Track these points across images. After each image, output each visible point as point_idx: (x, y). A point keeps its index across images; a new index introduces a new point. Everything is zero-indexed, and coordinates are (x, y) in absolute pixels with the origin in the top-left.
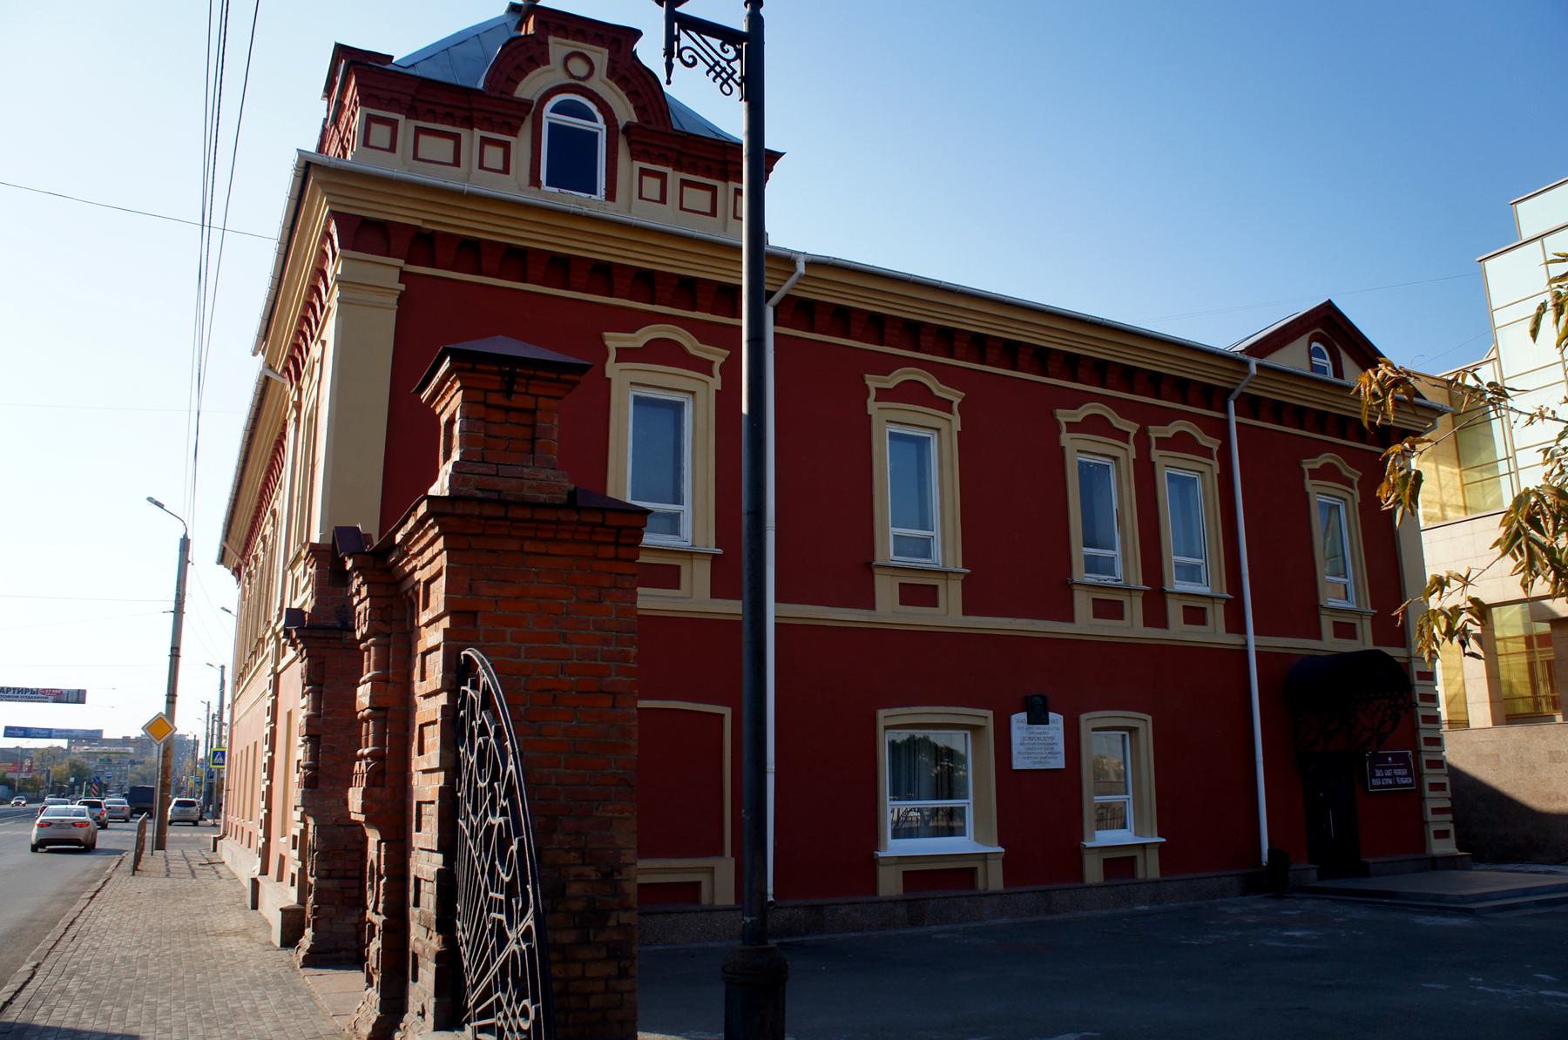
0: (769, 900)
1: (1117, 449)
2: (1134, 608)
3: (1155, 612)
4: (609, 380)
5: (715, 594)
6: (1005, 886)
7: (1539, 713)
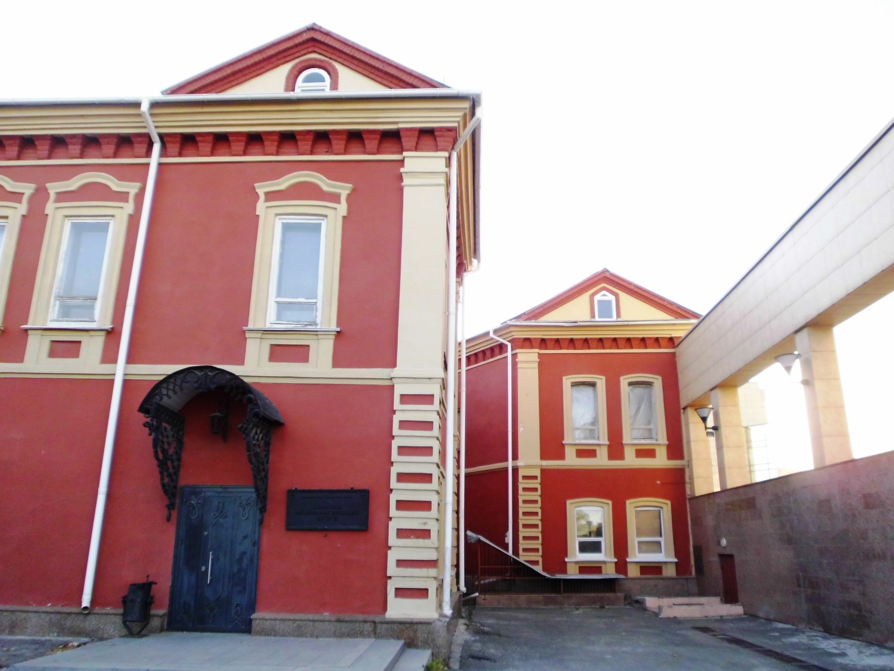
0: (48, 185)
5: (337, 363)
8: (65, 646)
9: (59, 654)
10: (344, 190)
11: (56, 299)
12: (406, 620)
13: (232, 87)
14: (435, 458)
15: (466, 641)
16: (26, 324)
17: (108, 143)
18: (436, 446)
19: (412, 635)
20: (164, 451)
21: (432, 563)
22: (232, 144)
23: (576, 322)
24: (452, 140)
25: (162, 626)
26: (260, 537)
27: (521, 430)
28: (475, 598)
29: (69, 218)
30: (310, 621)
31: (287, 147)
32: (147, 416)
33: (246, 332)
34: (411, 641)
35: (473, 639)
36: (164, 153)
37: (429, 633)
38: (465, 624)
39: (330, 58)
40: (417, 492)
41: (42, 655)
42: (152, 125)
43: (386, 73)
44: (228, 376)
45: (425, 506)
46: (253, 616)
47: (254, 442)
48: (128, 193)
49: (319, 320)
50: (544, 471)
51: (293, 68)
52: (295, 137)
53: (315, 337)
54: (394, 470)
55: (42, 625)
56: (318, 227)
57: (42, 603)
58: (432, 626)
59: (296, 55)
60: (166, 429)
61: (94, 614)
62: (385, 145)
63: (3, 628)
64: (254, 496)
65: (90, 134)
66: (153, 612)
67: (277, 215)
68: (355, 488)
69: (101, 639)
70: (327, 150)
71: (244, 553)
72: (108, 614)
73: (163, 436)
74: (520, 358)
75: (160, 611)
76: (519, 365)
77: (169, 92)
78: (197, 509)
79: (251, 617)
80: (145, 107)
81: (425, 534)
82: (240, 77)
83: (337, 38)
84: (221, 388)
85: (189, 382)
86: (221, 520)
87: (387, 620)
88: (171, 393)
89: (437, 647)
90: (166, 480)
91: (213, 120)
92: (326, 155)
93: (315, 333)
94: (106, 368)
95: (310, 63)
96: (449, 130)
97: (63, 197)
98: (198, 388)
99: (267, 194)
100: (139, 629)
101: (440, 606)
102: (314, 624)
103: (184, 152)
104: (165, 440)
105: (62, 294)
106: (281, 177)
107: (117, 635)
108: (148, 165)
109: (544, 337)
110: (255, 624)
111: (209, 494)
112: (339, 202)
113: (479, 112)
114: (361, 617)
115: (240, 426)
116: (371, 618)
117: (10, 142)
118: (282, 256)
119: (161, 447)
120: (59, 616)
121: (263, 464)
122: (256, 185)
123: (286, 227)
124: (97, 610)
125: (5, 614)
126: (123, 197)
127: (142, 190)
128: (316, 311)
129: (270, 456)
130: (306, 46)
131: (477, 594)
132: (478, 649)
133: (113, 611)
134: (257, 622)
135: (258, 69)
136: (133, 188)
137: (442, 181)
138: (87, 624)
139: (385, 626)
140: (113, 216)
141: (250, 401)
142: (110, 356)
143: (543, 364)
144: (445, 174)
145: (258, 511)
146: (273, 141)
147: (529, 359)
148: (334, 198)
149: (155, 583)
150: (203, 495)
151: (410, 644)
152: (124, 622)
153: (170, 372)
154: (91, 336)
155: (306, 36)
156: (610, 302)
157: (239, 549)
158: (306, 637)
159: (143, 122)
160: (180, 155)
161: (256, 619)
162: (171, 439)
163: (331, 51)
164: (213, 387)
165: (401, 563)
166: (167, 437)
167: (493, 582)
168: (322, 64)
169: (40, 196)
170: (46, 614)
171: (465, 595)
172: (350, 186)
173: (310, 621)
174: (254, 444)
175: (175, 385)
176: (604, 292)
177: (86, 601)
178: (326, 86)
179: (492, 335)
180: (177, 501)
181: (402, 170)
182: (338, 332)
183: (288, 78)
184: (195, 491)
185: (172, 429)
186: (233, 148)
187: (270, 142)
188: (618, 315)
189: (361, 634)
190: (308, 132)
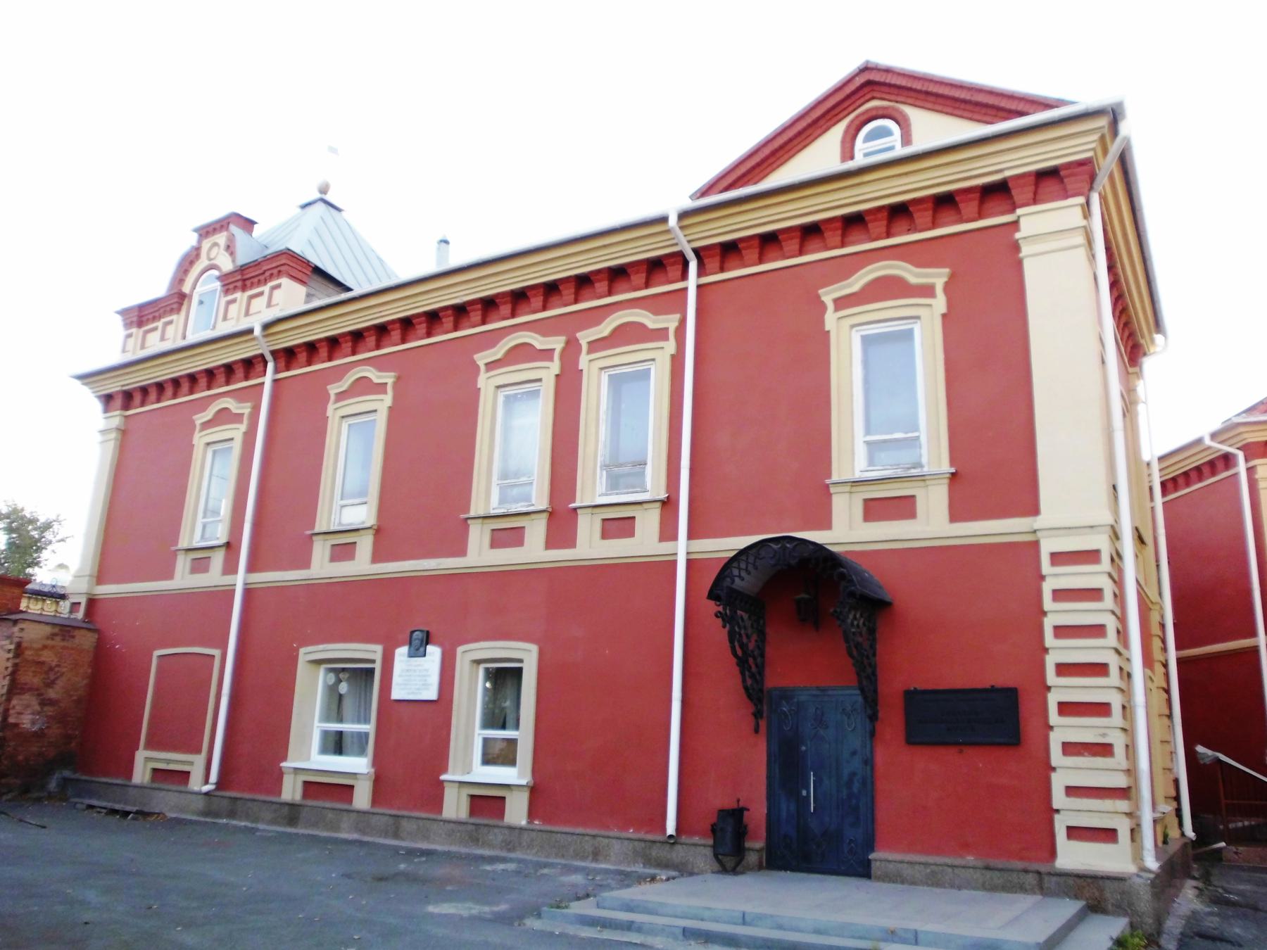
0: (579, 335)
2: (536, 531)
4: (194, 445)
5: (955, 516)
8: (653, 879)
9: (647, 887)
10: (938, 277)
11: (601, 470)
12: (1086, 873)
13: (774, 170)
14: (1111, 639)
15: (1194, 913)
16: (574, 502)
17: (637, 273)
18: (1111, 624)
19: (1097, 894)
20: (742, 646)
21: (1122, 793)
22: (783, 244)
24: (1087, 177)
25: (761, 862)
26: (872, 752)
28: (1220, 850)
29: (606, 370)
30: (948, 866)
31: (855, 234)
32: (718, 603)
33: (830, 486)
34: (1096, 903)
35: (1208, 909)
36: (702, 272)
37: (1123, 893)
38: (1196, 888)
39: (897, 102)
40: (1071, 690)
41: (628, 886)
42: (684, 240)
43: (977, 104)
44: (811, 547)
45: (1102, 709)
46: (872, 856)
47: (853, 630)
48: (667, 329)
49: (924, 460)
51: (849, 127)
52: (954, 199)
53: (922, 484)
54: (1051, 661)
55: (626, 854)
56: (908, 335)
57: (624, 828)
58: (1127, 884)
60: (742, 617)
61: (681, 844)
62: (989, 205)
63: (586, 854)
64: (860, 699)
65: (616, 266)
66: (748, 844)
67: (853, 326)
69: (691, 874)
70: (909, 228)
71: (853, 774)
72: (695, 845)
73: (739, 627)
75: (756, 844)
76: (1262, 485)
77: (698, 195)
78: (790, 718)
80: (673, 221)
81: (1104, 749)
82: (783, 156)
83: (902, 72)
84: (804, 562)
85: (764, 558)
86: (822, 732)
87: (1058, 871)
88: (743, 574)
89: (1138, 915)
90: (749, 682)
91: (760, 218)
92: (908, 234)
93: (922, 478)
94: (666, 547)
95: (871, 114)
96: (1081, 163)
97: (595, 346)
98: (775, 565)
99: (836, 301)
100: (733, 865)
101: (1138, 856)
102: (953, 870)
103: (727, 265)
104: (743, 632)
105: (608, 462)
107: (709, 871)
108: (685, 290)
110: (875, 866)
111: (803, 698)
113: (1125, 128)
114: (1019, 864)
115: (831, 610)
116: (1035, 866)
117: (534, 292)
118: (866, 381)
119: (739, 641)
120: (643, 845)
121: (868, 657)
123: (866, 340)
124: (684, 839)
125: (587, 838)
126: (661, 334)
127: (683, 322)
128: (920, 448)
129: (877, 647)
130: (861, 93)
131: (1223, 844)
132: (1212, 925)
133: (702, 842)
134: (878, 863)
136: (670, 322)
137: (1080, 239)
138: (674, 855)
139: (1054, 879)
140: (653, 360)
141: (842, 576)
144: (1083, 229)
145: (868, 720)
146: (835, 229)
148: (927, 291)
149: (748, 810)
150: (796, 700)
151: (1096, 907)
152: (716, 856)
153: (742, 546)
154: (646, 509)
155: (859, 81)
157: (846, 772)
158: (945, 887)
159: (673, 239)
160: (722, 269)
161: (876, 860)
162: (750, 631)
163: (896, 91)
164: (793, 562)
165: (1071, 791)
166: (745, 628)
167: (1251, 827)
168: (885, 112)
169: (572, 348)
170: (629, 841)
171: (1195, 844)
172: (946, 271)
173: (948, 866)
174: (854, 633)
175: (747, 563)
177: (671, 828)
178: (896, 141)
179: (1208, 442)
180: (765, 708)
181: (1018, 235)
182: (953, 474)
183: (843, 142)
184: (785, 695)
185: (749, 617)
186: (786, 249)
187: (830, 233)
189: (1022, 889)
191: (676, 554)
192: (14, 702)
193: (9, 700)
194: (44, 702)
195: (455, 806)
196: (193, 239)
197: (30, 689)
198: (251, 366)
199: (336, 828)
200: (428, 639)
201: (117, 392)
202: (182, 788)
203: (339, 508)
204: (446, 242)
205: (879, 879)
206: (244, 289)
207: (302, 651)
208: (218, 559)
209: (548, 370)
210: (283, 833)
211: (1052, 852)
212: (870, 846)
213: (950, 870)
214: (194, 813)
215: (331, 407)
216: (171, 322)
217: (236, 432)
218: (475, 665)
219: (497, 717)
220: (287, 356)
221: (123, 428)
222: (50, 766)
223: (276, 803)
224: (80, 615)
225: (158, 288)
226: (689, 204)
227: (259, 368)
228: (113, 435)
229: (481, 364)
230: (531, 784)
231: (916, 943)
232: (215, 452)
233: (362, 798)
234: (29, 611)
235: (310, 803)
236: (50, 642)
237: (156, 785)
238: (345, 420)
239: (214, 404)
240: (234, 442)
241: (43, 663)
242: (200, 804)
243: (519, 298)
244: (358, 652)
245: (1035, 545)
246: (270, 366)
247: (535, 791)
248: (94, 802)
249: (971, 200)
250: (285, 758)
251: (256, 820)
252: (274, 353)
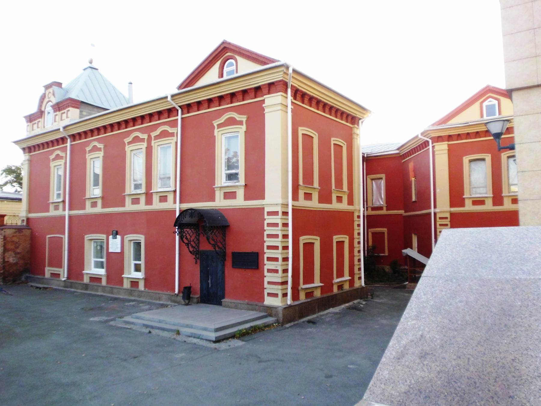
0: (151, 134)
1: (59, 163)
2: (143, 199)
3: (149, 201)
6: (107, 284)
7: (96, 242)
23: (468, 123)
27: (438, 191)
28: (405, 285)
50: (452, 214)
57: (167, 291)
58: (277, 309)
59: (221, 56)
67: (222, 134)
68: (254, 252)
74: (437, 148)
75: (196, 296)
76: (436, 153)
79: (222, 300)
95: (227, 58)
106: (221, 117)
108: (177, 119)
109: (450, 134)
110: (223, 303)
112: (242, 125)
122: (213, 122)
130: (223, 51)
131: (407, 283)
135: (208, 67)
142: (175, 202)
143: (451, 151)
147: (442, 148)
155: (222, 47)
156: (494, 106)
158: (238, 309)
165: (269, 283)
176: (490, 99)
179: (420, 136)
181: (264, 105)
188: (500, 113)
190: (227, 94)
191: (176, 208)
192: (6, 254)
193: (4, 254)
194: (16, 253)
195: (127, 285)
196: (43, 90)
197: (11, 250)
198: (63, 140)
199: (97, 290)
200: (117, 233)
201: (26, 147)
202: (58, 279)
203: (92, 189)
204: (131, 83)
205: (224, 307)
206: (59, 110)
207: (86, 236)
208: (61, 206)
209: (143, 145)
210: (82, 293)
211: (263, 299)
212: (223, 297)
213: (240, 304)
214: (61, 287)
215: (87, 155)
216: (39, 121)
217: (62, 162)
218: (130, 241)
219: (137, 257)
220: (73, 137)
221: (30, 159)
222: (21, 273)
223: (82, 284)
224: (25, 224)
225: (34, 109)
226: (176, 91)
227: (66, 140)
228: (27, 162)
229: (126, 142)
230: (144, 278)
231: (192, 328)
232: (58, 169)
233: (104, 282)
234: (8, 224)
235: (91, 283)
236: (15, 234)
237: (51, 278)
238: (91, 160)
239: (55, 152)
240: (62, 166)
241: (13, 241)
242: (62, 284)
243: (134, 120)
244: (338, 142)
245: (263, 208)
246: (69, 140)
247: (146, 280)
248: (33, 284)
249: (252, 92)
250: (84, 270)
251: (77, 289)
252: (69, 136)
